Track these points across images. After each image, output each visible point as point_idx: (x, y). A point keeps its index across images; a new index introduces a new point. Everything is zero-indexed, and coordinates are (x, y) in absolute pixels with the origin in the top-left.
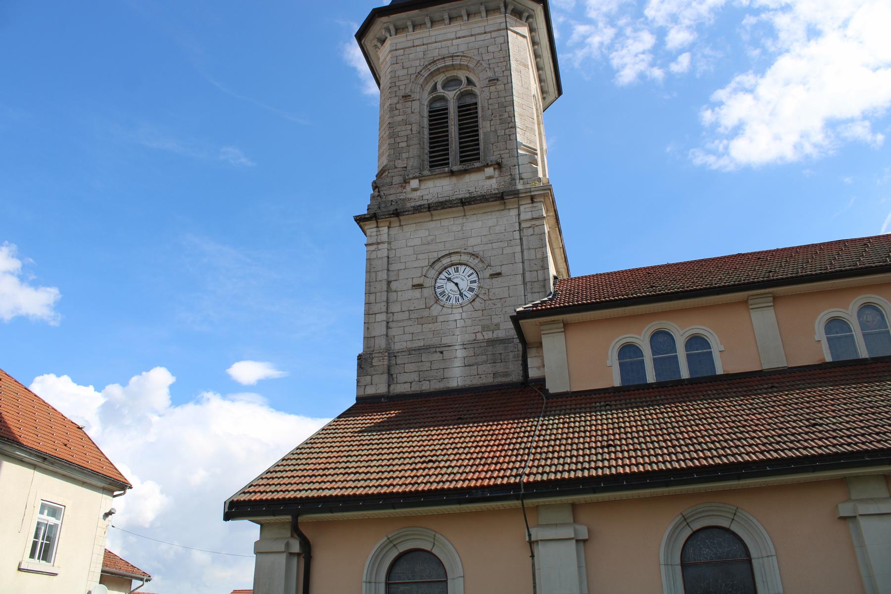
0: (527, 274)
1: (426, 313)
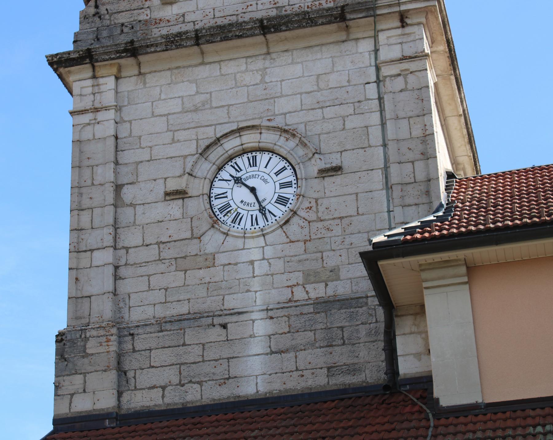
0: (394, 169)
1: (193, 248)
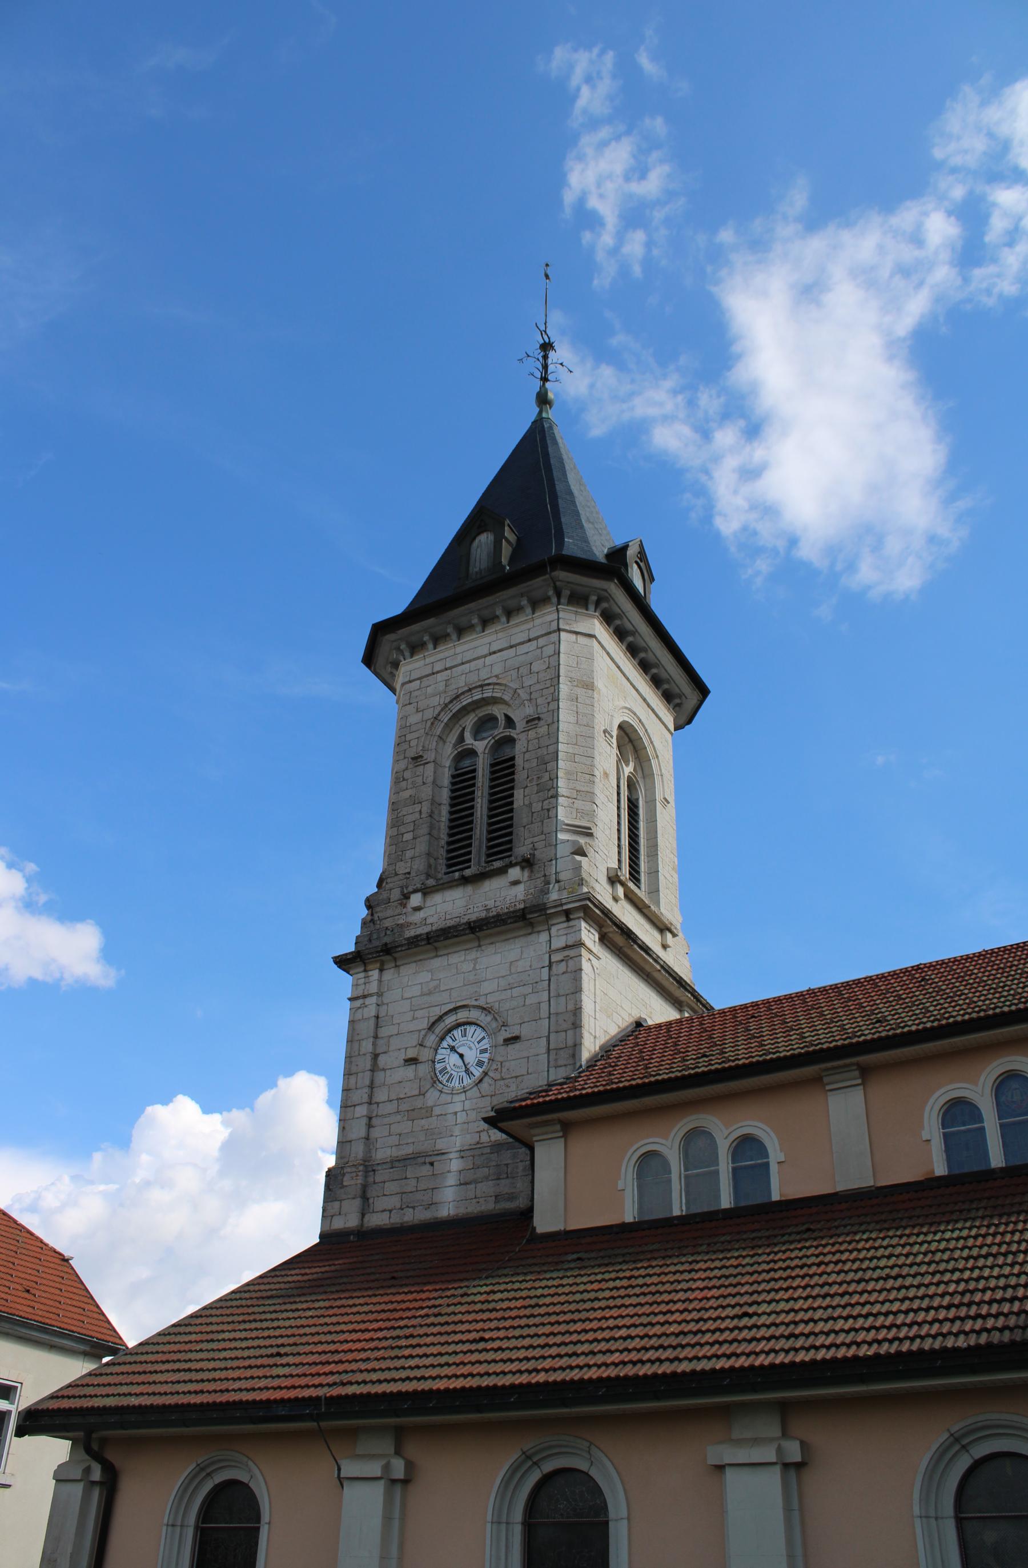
0: (553, 1036)
1: (419, 1103)
